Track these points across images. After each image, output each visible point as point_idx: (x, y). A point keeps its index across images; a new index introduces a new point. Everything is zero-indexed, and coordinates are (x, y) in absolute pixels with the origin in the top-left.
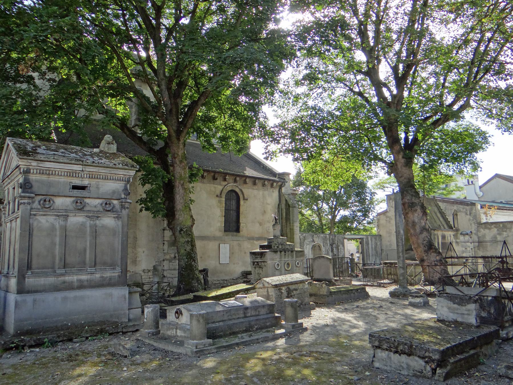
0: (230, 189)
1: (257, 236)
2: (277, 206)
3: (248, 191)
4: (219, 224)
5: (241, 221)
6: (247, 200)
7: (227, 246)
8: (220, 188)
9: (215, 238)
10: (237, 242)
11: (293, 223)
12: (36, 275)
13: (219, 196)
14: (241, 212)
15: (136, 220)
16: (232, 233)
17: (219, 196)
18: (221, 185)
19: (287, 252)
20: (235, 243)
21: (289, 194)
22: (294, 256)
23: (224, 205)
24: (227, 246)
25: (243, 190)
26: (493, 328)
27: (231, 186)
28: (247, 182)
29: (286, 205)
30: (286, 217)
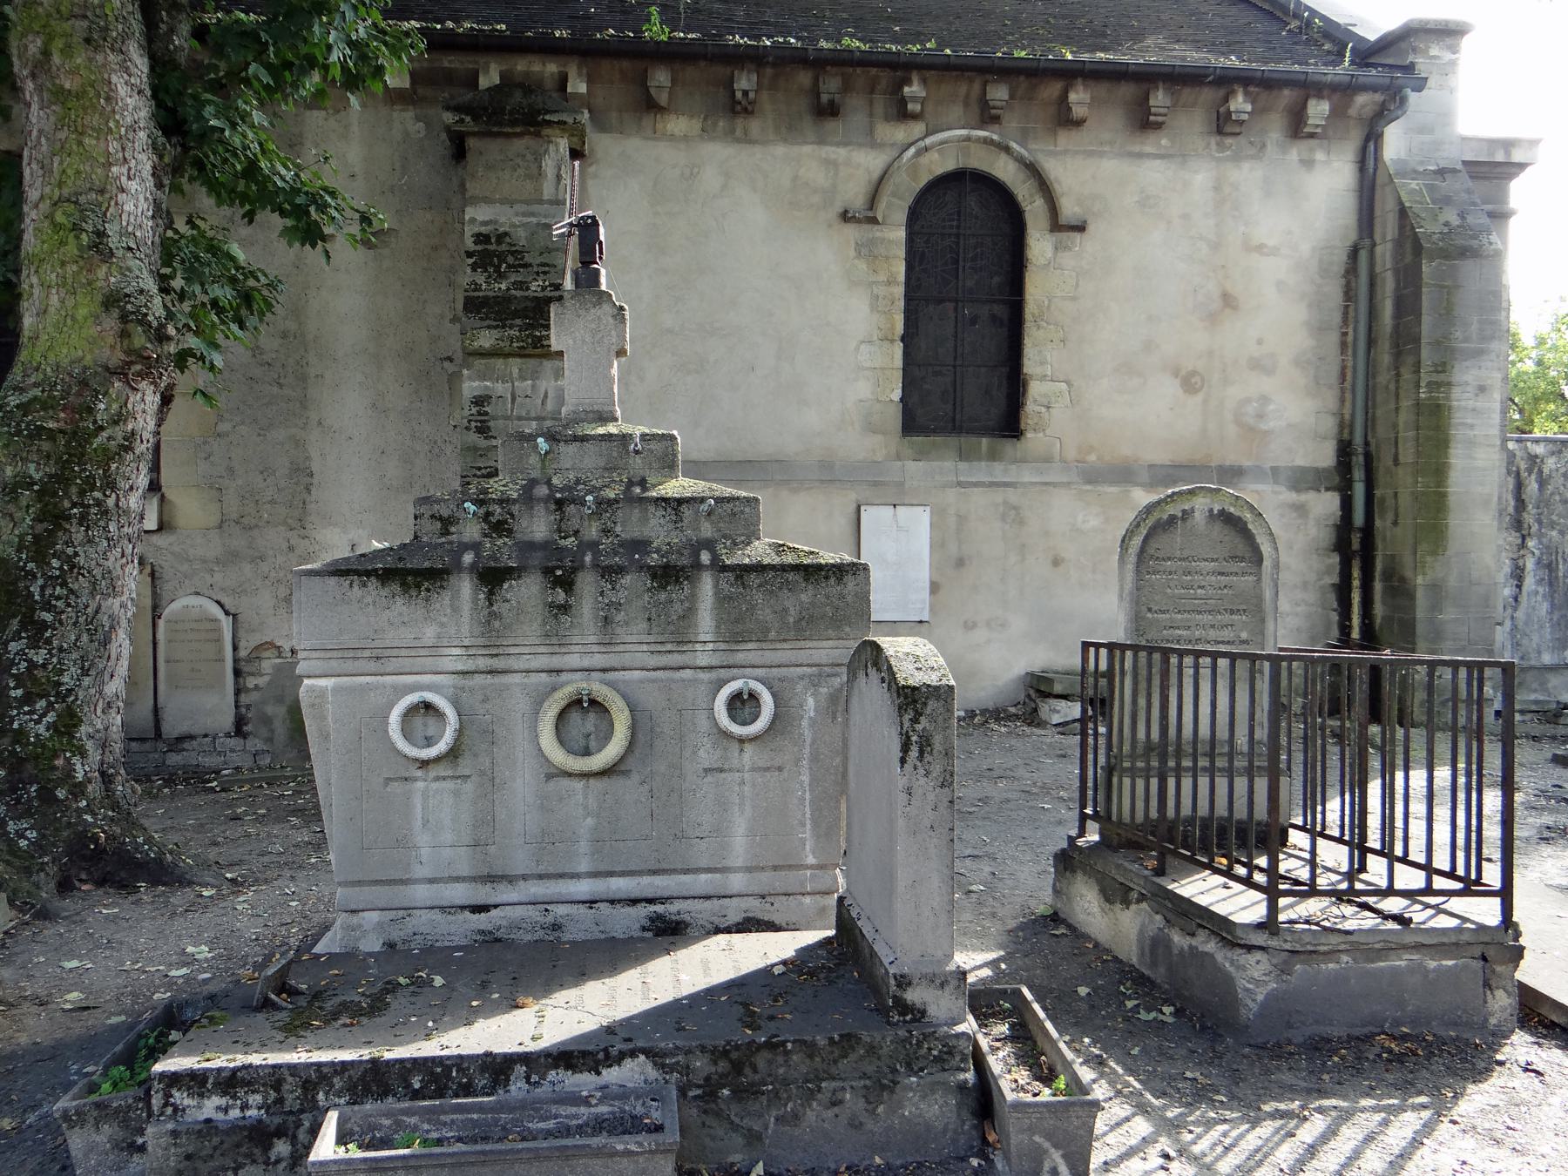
0: (950, 165)
1: (1161, 457)
2: (1340, 258)
3: (1092, 170)
4: (864, 388)
5: (1030, 365)
6: (1080, 228)
7: (919, 520)
8: (870, 162)
9: (828, 473)
10: (998, 496)
11: (1442, 367)
12: (722, 599)
13: (862, 216)
14: (1030, 309)
15: (303, 378)
16: (967, 441)
17: (862, 216)
18: (874, 145)
19: (587, 583)
20: (979, 500)
21: (1441, 172)
22: (706, 621)
23: (901, 269)
24: (919, 520)
25: (1054, 169)
27: (946, 144)
28: (1078, 111)
29: (1399, 244)
30: (1396, 327)
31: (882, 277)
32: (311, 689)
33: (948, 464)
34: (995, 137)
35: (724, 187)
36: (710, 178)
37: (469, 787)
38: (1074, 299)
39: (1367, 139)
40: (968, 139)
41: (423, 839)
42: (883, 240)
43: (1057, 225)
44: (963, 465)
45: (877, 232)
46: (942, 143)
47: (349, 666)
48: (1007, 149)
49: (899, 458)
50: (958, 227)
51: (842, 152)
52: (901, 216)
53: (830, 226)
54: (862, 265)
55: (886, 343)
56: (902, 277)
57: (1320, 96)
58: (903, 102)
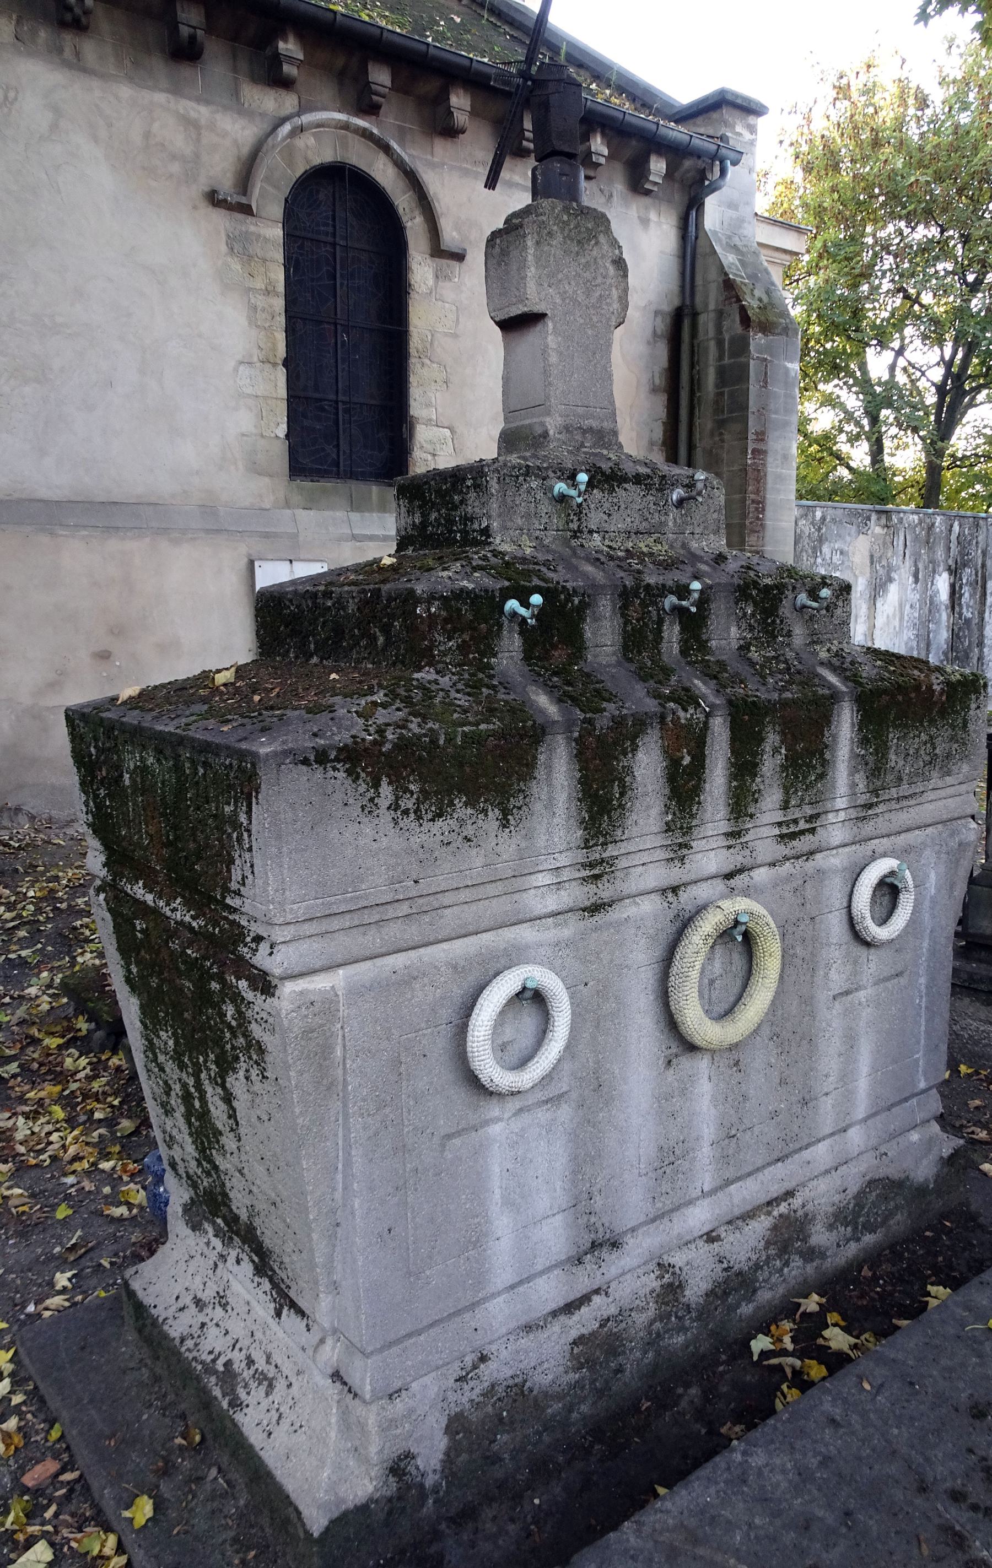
2: (662, 326)
4: (244, 421)
5: (417, 408)
14: (415, 343)
16: (356, 487)
17: (232, 201)
23: (279, 276)
26: (790, 1375)
31: (259, 284)
32: (307, 1002)
33: (340, 514)
34: (375, 131)
35: (54, 127)
36: (32, 109)
37: (565, 1112)
38: (455, 336)
39: (689, 208)
40: (346, 126)
41: (502, 1224)
42: (259, 236)
43: (438, 251)
44: (355, 516)
45: (251, 226)
46: (320, 125)
47: (372, 940)
48: (387, 149)
49: (288, 505)
50: (334, 235)
51: (202, 112)
52: (276, 210)
53: (195, 208)
54: (236, 266)
55: (268, 366)
56: (281, 288)
57: (659, 154)
58: (277, 60)
